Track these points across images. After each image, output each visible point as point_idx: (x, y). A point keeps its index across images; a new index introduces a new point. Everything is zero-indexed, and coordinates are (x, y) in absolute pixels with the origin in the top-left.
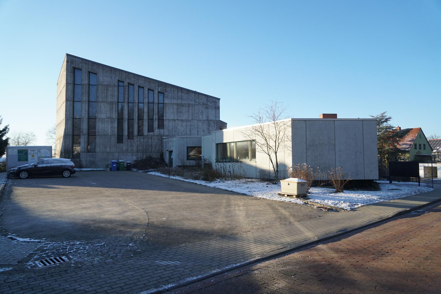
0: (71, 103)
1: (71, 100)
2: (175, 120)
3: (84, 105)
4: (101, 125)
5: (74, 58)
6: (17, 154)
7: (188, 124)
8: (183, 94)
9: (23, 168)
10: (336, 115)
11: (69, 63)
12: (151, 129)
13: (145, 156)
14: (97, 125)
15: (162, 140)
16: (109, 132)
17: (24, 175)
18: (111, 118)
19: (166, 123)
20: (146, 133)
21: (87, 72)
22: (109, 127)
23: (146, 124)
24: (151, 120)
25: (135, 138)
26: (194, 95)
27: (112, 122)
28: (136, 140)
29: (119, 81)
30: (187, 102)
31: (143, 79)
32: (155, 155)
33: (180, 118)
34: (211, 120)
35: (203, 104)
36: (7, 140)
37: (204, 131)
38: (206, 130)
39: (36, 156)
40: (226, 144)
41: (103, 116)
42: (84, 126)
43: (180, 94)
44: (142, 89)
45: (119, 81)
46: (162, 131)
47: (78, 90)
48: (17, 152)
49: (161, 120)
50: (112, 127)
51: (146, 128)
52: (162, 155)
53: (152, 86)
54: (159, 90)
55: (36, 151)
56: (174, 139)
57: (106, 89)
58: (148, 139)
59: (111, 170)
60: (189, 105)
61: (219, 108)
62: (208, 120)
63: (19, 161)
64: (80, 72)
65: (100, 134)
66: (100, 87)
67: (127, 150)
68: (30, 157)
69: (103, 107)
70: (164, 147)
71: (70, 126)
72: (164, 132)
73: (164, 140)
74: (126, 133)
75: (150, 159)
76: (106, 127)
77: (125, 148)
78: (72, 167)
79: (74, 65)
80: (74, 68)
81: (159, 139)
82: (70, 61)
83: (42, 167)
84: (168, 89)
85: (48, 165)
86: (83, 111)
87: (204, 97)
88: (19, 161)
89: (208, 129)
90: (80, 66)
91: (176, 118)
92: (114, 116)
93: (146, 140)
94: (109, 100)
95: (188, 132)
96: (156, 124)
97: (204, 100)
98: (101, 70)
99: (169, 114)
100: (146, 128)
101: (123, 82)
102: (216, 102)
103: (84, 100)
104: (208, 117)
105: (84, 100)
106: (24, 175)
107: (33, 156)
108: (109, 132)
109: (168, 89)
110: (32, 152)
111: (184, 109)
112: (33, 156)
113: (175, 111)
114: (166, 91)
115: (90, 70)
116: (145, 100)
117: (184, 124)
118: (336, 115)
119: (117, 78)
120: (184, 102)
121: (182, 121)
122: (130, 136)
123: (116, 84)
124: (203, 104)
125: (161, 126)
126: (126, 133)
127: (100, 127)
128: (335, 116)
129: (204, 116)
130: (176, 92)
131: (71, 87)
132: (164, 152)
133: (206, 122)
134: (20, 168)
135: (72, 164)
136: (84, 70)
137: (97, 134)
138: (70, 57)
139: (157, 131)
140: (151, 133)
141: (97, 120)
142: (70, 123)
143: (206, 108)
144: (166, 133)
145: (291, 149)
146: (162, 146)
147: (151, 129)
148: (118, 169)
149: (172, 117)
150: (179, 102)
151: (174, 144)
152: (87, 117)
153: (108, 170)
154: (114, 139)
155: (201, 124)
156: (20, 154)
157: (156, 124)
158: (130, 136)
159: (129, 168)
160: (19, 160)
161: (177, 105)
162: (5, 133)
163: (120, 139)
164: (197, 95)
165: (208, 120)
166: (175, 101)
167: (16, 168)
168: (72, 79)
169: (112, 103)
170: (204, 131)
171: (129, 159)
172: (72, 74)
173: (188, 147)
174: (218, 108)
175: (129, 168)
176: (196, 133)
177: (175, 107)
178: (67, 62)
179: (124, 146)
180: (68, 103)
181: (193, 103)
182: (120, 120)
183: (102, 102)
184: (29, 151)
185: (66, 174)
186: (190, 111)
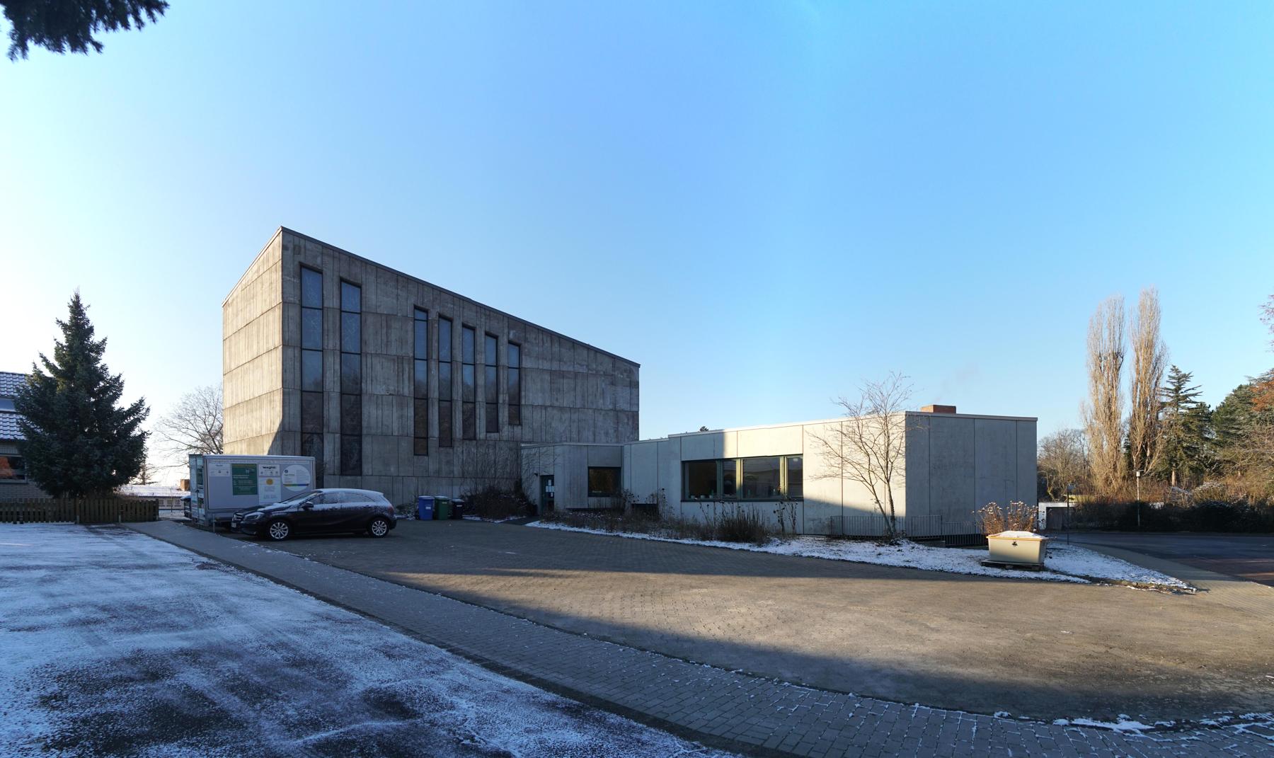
0: (297, 352)
1: (296, 345)
2: (546, 408)
3: (331, 359)
4: (374, 412)
5: (302, 242)
6: (230, 474)
7: (575, 416)
8: (563, 350)
9: (277, 513)
10: (954, 408)
11: (290, 252)
12: (494, 426)
13: (480, 488)
14: (365, 410)
15: (517, 451)
16: (395, 429)
17: (279, 531)
18: (399, 395)
19: (526, 413)
20: (482, 434)
21: (336, 280)
22: (395, 415)
23: (481, 413)
24: (493, 404)
25: (457, 444)
26: (585, 352)
27: (401, 406)
28: (460, 450)
29: (416, 307)
30: (571, 369)
31: (474, 308)
32: (505, 486)
33: (556, 404)
34: (623, 411)
35: (605, 374)
36: (142, 436)
37: (607, 434)
38: (611, 431)
39: (277, 484)
40: (732, 460)
41: (380, 389)
42: (333, 411)
43: (556, 348)
44: (471, 332)
45: (416, 307)
46: (517, 430)
47: (313, 321)
48: (230, 470)
49: (516, 405)
50: (402, 416)
51: (481, 424)
52: (519, 484)
53: (495, 327)
54: (511, 336)
55: (278, 469)
56: (559, 450)
57: (384, 324)
58: (488, 447)
59: (418, 517)
60: (576, 375)
61: (636, 385)
62: (614, 410)
63: (235, 494)
64: (318, 278)
65: (373, 431)
66: (370, 319)
67: (438, 472)
68: (262, 484)
69: (378, 367)
70: (525, 467)
71: (295, 409)
72: (524, 432)
73: (524, 452)
74: (435, 432)
75: (492, 493)
76: (386, 416)
77: (433, 467)
78: (390, 511)
79: (301, 258)
80: (302, 266)
81: (511, 449)
82: (291, 246)
83: (323, 511)
84: (531, 337)
85: (337, 506)
86: (329, 374)
87: (607, 359)
88: (235, 494)
89: (616, 430)
90: (319, 260)
91: (548, 404)
92: (406, 392)
93: (482, 450)
94: (393, 351)
95: (574, 435)
96: (504, 415)
97: (608, 365)
98: (372, 278)
99: (534, 394)
100: (481, 424)
101: (426, 311)
102: (631, 371)
103: (331, 346)
104: (615, 405)
105: (331, 346)
106: (279, 531)
107: (270, 482)
108: (395, 429)
109: (531, 337)
110: (268, 472)
111: (566, 384)
112: (270, 482)
113: (547, 386)
114: (526, 340)
115: (344, 275)
116: (478, 357)
117: (566, 416)
118: (954, 408)
119: (412, 301)
120: (564, 368)
121: (561, 409)
122: (447, 440)
123: (411, 315)
124: (605, 374)
125: (516, 419)
126: (435, 432)
127: (372, 414)
128: (953, 409)
129: (608, 401)
130: (548, 344)
131: (294, 312)
132: (524, 477)
133: (611, 414)
134: (269, 512)
135: (387, 504)
136: (328, 272)
137: (364, 432)
138: (290, 238)
139: (506, 431)
140: (494, 435)
141: (365, 398)
142: (296, 400)
143: (612, 384)
144: (528, 436)
145: (904, 473)
146: (519, 465)
147: (494, 426)
148: (435, 516)
149: (539, 402)
150: (555, 366)
151: (559, 460)
152: (338, 389)
153: (411, 518)
154: (407, 446)
155: (601, 418)
156: (236, 477)
157: (504, 415)
158: (447, 440)
159: (456, 512)
160: (236, 491)
161: (551, 372)
162: (139, 420)
163: (420, 444)
164: (592, 354)
165: (614, 410)
166: (547, 365)
167: (258, 514)
168: (298, 292)
169: (400, 359)
170: (607, 434)
171: (453, 493)
172: (297, 281)
173: (683, 463)
174: (634, 385)
175: (456, 512)
176: (591, 438)
177: (547, 377)
178: (284, 248)
179: (432, 463)
180: (290, 351)
181: (584, 370)
182: (421, 400)
183: (377, 355)
184: (260, 469)
185: (379, 528)
186: (578, 389)
